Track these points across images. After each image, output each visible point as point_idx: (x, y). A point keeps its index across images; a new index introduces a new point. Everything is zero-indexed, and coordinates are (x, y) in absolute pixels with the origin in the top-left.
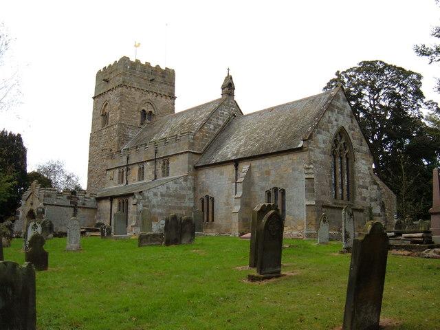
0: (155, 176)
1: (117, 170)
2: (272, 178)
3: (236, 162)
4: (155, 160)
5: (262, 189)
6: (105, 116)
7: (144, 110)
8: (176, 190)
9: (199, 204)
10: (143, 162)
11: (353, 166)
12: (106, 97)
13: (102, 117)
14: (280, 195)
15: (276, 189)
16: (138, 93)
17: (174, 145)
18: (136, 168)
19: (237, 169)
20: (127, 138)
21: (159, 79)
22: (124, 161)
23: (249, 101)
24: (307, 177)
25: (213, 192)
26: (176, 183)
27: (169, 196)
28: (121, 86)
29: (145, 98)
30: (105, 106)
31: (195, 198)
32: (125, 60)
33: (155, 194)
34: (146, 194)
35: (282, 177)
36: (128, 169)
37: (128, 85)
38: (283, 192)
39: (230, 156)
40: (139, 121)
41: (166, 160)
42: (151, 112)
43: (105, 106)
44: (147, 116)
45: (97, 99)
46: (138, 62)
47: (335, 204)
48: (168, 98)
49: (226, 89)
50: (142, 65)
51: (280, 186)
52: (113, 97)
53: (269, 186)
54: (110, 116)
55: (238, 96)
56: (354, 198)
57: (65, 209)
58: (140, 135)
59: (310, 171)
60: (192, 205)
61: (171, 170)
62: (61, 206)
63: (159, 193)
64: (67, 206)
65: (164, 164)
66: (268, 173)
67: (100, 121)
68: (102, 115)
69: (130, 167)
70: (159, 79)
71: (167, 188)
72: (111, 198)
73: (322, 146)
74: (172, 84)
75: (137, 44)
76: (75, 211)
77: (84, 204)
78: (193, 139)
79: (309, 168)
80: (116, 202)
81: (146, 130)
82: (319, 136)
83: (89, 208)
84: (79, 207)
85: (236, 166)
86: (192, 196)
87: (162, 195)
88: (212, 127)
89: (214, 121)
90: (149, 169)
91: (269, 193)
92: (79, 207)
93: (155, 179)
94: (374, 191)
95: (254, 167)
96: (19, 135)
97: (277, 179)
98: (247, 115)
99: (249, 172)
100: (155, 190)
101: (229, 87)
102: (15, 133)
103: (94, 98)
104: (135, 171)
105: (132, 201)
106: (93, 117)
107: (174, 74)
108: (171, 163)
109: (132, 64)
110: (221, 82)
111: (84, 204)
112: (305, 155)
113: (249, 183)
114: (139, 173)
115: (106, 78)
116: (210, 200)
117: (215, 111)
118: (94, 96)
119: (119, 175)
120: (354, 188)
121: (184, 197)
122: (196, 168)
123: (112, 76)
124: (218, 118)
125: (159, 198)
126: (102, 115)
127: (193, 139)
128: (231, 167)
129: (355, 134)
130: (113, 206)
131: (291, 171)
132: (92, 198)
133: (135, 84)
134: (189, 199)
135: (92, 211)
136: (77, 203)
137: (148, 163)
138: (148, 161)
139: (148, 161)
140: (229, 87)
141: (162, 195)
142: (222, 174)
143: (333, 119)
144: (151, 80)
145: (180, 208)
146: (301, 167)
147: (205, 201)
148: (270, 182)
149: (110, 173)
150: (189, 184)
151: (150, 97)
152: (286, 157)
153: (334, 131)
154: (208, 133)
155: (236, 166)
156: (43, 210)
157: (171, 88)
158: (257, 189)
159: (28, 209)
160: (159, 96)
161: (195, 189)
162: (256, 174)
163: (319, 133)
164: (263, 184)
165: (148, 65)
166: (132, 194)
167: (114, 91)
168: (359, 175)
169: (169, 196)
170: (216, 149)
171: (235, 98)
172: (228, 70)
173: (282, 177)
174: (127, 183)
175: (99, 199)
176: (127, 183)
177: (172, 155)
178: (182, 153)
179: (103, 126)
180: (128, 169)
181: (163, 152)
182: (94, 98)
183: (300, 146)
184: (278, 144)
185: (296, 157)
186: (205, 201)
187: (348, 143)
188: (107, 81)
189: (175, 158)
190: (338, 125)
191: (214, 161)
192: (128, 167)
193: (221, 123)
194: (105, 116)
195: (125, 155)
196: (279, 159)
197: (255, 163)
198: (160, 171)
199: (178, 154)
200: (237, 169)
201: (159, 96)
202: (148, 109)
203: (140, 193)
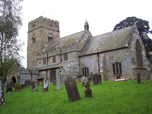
0: (61, 61)
1: (42, 60)
2: (114, 59)
3: (98, 54)
4: (60, 55)
5: (111, 63)
6: (34, 39)
7: (49, 36)
8: (73, 66)
9: (82, 70)
10: (55, 56)
11: (141, 53)
12: (34, 32)
13: (32, 40)
14: (119, 65)
15: (117, 63)
16: (47, 30)
17: (69, 48)
18: (52, 58)
19: (98, 57)
20: (44, 47)
21: (54, 25)
22: (46, 56)
23: (95, 32)
24: (131, 57)
25: (88, 65)
26: (73, 63)
27: (71, 68)
28: (41, 27)
29: (49, 32)
30: (33, 36)
31: (80, 68)
32: (41, 18)
33: (67, 67)
34: (64, 67)
35: (119, 58)
36: (48, 59)
37: (43, 27)
38: (120, 64)
39: (94, 52)
40: (47, 41)
41: (66, 54)
42: (51, 37)
43: (33, 36)
44: (50, 39)
45: (29, 33)
46: (46, 18)
47: (139, 67)
48: (57, 32)
49: (86, 27)
50: (47, 19)
51: (119, 61)
52: (37, 32)
53: (114, 61)
54: (36, 39)
55: (90, 29)
56: (143, 65)
57: (28, 75)
58: (49, 46)
59: (132, 55)
60: (79, 71)
61: (68, 58)
62: (26, 74)
63: (68, 67)
64: (28, 74)
65: (65, 56)
66: (113, 57)
67: (32, 41)
68: (32, 39)
69: (49, 58)
70: (54, 25)
71: (71, 65)
72: (47, 70)
73: (133, 46)
74: (58, 27)
75: (44, 12)
76: (32, 75)
77: (35, 73)
78: (78, 46)
79: (131, 54)
80: (49, 71)
81: (51, 44)
82: (132, 42)
83: (36, 74)
84: (33, 74)
85: (98, 55)
86: (79, 67)
87: (69, 68)
88: (83, 41)
89: (83, 39)
90: (58, 59)
91: (114, 65)
92: (33, 74)
93: (61, 62)
94: (148, 62)
95: (106, 55)
96: (148, 22)
97: (117, 59)
98: (95, 37)
99: (104, 58)
100: (66, 66)
101: (87, 26)
102: (147, 21)
103: (28, 32)
104: (51, 59)
105: (57, 71)
106: (28, 39)
107: (59, 23)
108: (68, 55)
109: (44, 19)
110: (84, 25)
111: (35, 73)
112: (129, 50)
113: (105, 62)
114: (53, 60)
115: (33, 24)
116: (86, 69)
117: (83, 35)
118: (28, 32)
119: (43, 62)
120: (142, 61)
121: (76, 68)
122: (79, 57)
123: (36, 24)
124: (85, 38)
125: (68, 69)
126: (32, 39)
127: (78, 46)
128: (96, 56)
129: (141, 41)
130: (48, 73)
131: (123, 56)
132: (38, 70)
133: (46, 27)
134: (78, 69)
135: (38, 75)
136: (32, 73)
137: (57, 56)
138: (57, 55)
139: (57, 55)
140: (87, 26)
141: (69, 68)
142: (91, 58)
143: (135, 36)
144: (51, 25)
145: (75, 72)
146: (127, 54)
147: (84, 69)
148: (114, 61)
149: (39, 61)
150: (77, 63)
151: (51, 31)
152: (120, 51)
153: (136, 40)
154: (82, 43)
155: (98, 55)
156: (20, 76)
157: (58, 28)
158: (108, 63)
159: (12, 76)
160: (54, 31)
161: (79, 65)
162: (107, 58)
163: (132, 41)
164: (111, 61)
165: (49, 19)
166: (58, 68)
167: (37, 29)
168: (143, 57)
169: (71, 68)
170: (86, 50)
171: (90, 30)
172: (86, 20)
173: (119, 58)
174: (48, 64)
175: (40, 71)
176: (48, 64)
177: (69, 52)
178: (73, 51)
179: (33, 43)
180: (48, 59)
181: (64, 51)
182: (28, 32)
183: (127, 46)
184: (115, 46)
185: (125, 50)
186: (84, 69)
187: (139, 45)
188: (34, 26)
189: (70, 53)
190: (136, 38)
191: (87, 54)
192: (48, 58)
193: (86, 39)
194: (34, 39)
195: (46, 53)
196: (117, 52)
197: (106, 54)
198: (63, 59)
199: (71, 52)
200: (98, 57)
201: (54, 31)
202: (51, 36)
203: (62, 67)
